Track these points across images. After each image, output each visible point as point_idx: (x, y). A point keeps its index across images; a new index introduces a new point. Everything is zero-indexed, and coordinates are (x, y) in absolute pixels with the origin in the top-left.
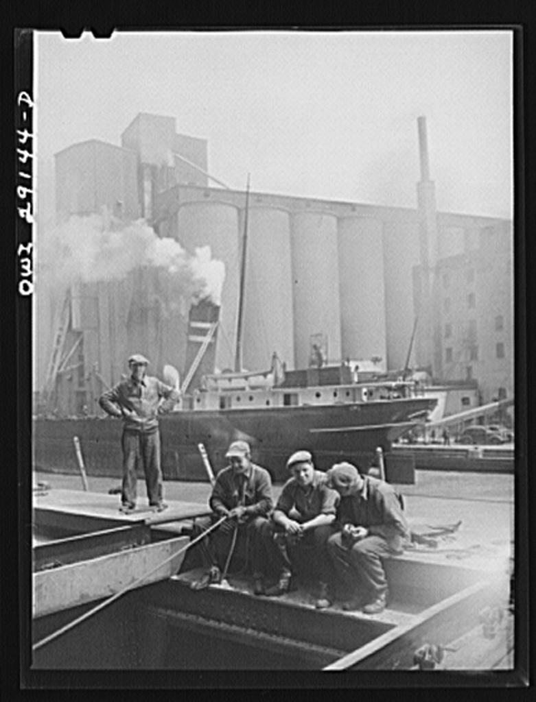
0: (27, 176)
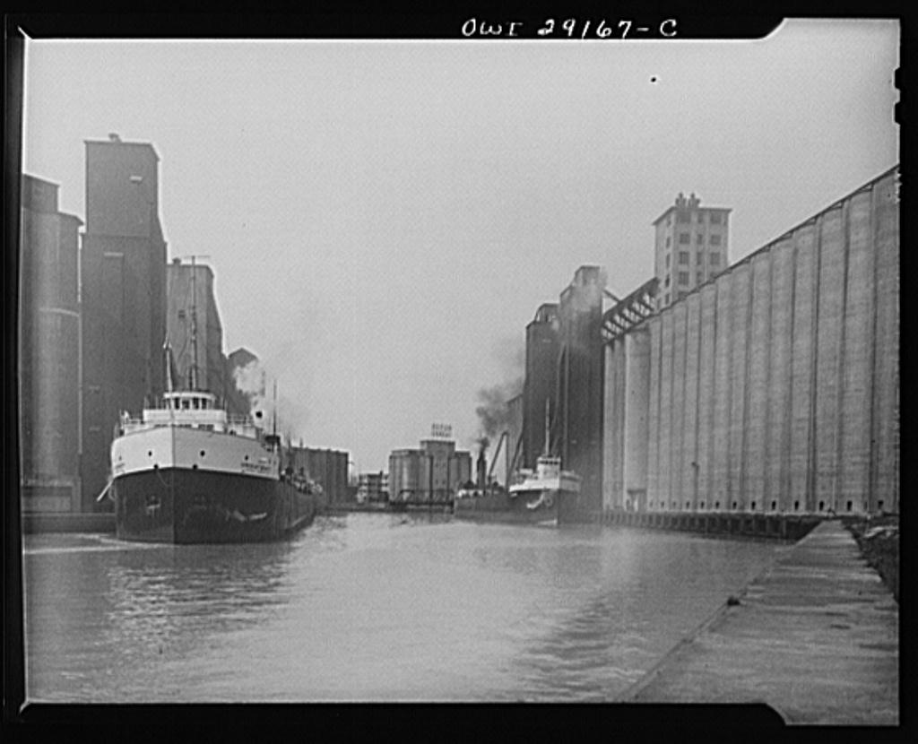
0: (584, 34)
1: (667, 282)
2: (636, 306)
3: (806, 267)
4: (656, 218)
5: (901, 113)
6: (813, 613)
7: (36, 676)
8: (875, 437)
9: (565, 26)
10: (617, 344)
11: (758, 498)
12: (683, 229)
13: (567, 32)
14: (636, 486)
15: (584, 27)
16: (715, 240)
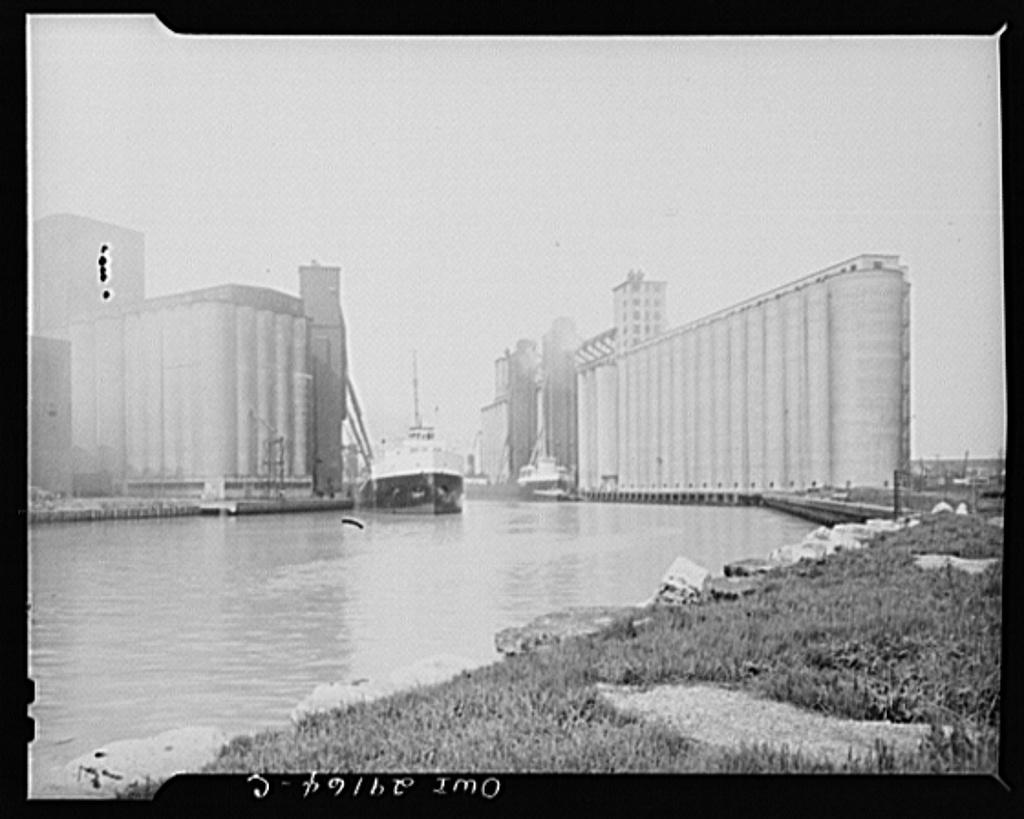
0: (361, 780)
1: (625, 331)
2: (598, 345)
3: (737, 340)
4: (617, 284)
5: (27, 691)
6: (235, 397)
7: (39, 596)
8: (321, 454)
9: (382, 789)
10: (589, 374)
11: (709, 481)
12: (636, 296)
13: (380, 783)
14: (609, 472)
15: (361, 788)
16: (657, 316)
